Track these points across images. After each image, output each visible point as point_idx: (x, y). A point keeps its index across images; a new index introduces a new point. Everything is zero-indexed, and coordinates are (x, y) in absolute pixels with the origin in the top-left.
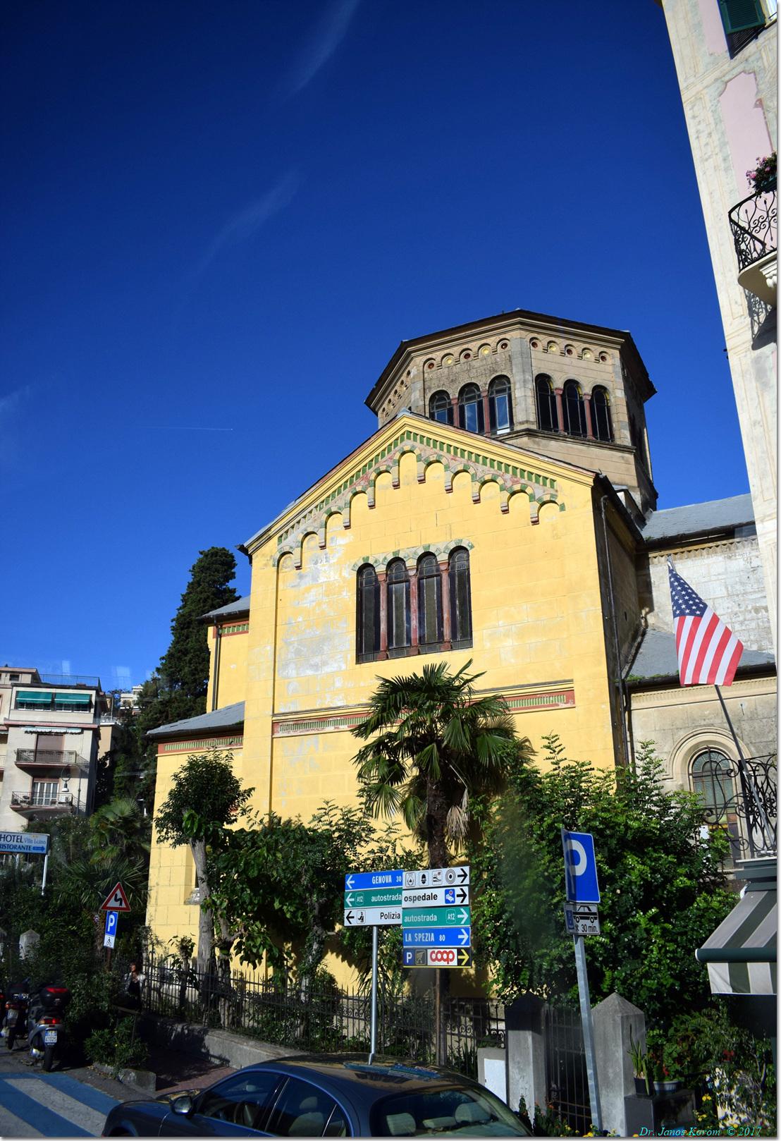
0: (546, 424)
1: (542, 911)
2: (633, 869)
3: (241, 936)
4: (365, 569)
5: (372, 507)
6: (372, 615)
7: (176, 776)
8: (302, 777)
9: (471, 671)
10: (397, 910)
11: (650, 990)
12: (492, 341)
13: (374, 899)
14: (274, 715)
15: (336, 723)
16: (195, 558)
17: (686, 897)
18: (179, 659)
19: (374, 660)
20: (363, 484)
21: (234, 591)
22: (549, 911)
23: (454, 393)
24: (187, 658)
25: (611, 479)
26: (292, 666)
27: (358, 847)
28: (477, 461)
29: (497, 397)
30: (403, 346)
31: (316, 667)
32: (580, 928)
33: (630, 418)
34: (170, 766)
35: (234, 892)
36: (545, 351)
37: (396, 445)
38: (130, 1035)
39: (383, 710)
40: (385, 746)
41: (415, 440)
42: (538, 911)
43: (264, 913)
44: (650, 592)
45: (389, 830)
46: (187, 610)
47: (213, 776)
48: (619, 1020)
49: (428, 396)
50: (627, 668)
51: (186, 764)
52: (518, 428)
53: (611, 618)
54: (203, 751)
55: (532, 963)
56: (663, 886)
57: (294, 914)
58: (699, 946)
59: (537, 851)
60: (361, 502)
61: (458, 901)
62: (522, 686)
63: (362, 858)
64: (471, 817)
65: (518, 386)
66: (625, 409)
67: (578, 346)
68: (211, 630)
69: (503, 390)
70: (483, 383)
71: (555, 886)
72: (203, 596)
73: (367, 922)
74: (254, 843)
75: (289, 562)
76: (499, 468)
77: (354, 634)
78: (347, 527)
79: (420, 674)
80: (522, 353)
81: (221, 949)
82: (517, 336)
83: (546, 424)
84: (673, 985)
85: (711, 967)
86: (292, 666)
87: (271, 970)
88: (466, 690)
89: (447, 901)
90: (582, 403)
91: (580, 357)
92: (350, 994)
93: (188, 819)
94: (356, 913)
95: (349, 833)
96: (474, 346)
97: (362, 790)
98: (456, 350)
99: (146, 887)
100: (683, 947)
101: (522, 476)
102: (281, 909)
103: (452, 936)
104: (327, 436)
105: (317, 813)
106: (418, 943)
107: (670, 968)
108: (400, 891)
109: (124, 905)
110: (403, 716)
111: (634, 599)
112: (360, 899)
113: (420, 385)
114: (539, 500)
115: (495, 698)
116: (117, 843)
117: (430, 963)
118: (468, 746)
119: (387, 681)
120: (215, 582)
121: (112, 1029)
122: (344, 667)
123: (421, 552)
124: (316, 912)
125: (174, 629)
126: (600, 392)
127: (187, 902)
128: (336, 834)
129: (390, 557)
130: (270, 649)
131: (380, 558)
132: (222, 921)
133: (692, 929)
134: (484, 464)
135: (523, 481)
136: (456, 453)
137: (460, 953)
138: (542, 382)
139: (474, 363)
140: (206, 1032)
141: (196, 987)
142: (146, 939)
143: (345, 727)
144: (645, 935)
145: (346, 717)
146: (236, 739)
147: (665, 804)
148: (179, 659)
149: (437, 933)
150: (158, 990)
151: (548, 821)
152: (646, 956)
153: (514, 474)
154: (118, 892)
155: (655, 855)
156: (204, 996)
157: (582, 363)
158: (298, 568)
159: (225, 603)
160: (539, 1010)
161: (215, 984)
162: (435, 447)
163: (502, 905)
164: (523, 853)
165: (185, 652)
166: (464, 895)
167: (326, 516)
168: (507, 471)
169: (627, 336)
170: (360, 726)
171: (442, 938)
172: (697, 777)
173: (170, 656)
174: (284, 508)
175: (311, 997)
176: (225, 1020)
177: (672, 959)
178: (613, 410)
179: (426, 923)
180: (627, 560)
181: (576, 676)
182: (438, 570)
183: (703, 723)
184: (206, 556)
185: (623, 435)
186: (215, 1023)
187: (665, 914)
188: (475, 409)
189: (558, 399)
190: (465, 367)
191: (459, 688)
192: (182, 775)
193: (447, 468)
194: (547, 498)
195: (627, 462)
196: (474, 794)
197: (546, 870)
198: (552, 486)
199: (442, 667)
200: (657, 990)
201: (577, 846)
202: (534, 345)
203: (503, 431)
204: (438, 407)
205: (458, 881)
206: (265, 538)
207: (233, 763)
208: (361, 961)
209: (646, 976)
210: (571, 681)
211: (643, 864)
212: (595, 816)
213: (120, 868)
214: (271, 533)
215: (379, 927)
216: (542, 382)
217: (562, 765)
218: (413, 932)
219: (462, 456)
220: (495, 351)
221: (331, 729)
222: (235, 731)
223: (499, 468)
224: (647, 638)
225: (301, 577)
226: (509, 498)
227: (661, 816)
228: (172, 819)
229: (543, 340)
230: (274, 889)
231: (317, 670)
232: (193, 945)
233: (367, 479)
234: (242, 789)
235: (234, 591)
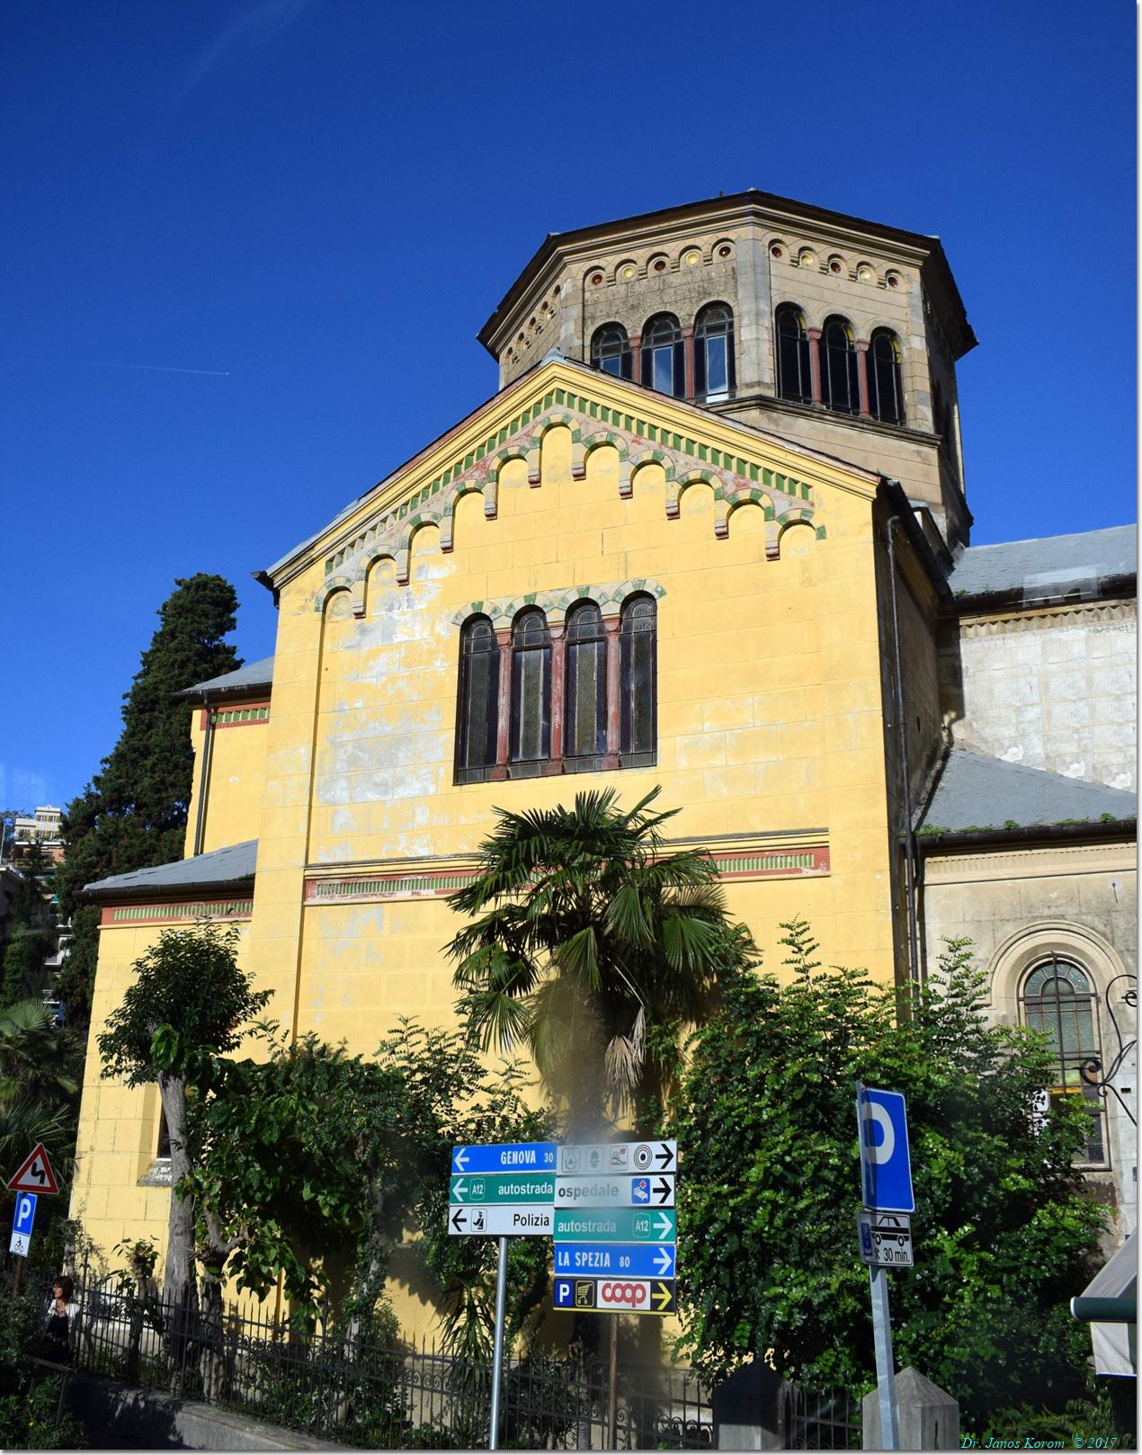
0: (791, 388)
1: (778, 1222)
2: (935, 1156)
3: (242, 1245)
4: (475, 623)
5: (491, 516)
6: (483, 703)
7: (139, 964)
8: (361, 977)
9: (658, 806)
10: (547, 1211)
11: (957, 1364)
12: (705, 241)
13: (502, 1190)
14: (307, 867)
15: (415, 885)
16: (167, 592)
17: (1021, 1208)
18: (134, 762)
19: (486, 779)
20: (478, 476)
21: (232, 651)
22: (788, 1223)
23: (634, 329)
24: (149, 762)
25: (907, 490)
26: (343, 783)
27: (455, 1100)
28: (676, 446)
29: (709, 339)
30: (550, 244)
31: (384, 787)
32: (882, 1255)
33: (933, 386)
34: (125, 950)
35: (232, 1167)
36: (795, 263)
37: (537, 412)
38: (53, 1408)
39: (506, 866)
40: (503, 926)
41: (570, 405)
42: (771, 1223)
43: (283, 1206)
44: (960, 685)
45: (510, 1072)
46: (150, 679)
47: (204, 967)
48: (917, 1413)
49: (591, 330)
50: (918, 812)
51: (157, 944)
52: (743, 393)
53: (896, 727)
54: (187, 923)
55: (756, 1311)
56: (980, 1188)
57: (335, 1210)
58: (1078, 1293)
59: (771, 1121)
60: (473, 507)
61: (656, 1199)
62: (740, 837)
63: (460, 1119)
64: (648, 1055)
65: (745, 321)
66: (926, 370)
67: (850, 258)
68: (198, 716)
69: (719, 328)
70: (686, 313)
71: (802, 1180)
72: (180, 656)
73: (489, 1230)
74: (271, 1088)
75: (343, 606)
76: (715, 461)
77: (453, 733)
78: (447, 550)
79: (570, 808)
80: (754, 266)
81: (208, 1265)
82: (747, 236)
83: (791, 388)
84: (995, 1357)
85: (1096, 1328)
86: (343, 783)
87: (285, 1305)
88: (648, 838)
89: (636, 1199)
90: (853, 357)
91: (853, 277)
92: (420, 1352)
93: (161, 1039)
94: (470, 1213)
95: (439, 1074)
96: (672, 249)
97: (465, 1003)
98: (641, 255)
99: (72, 1152)
100: (1011, 1293)
101: (754, 477)
102: (313, 1201)
103: (643, 1259)
104: (412, 394)
105: (390, 1038)
106: (580, 1270)
107: (991, 1329)
108: (550, 1179)
109: (47, 1184)
110: (536, 876)
111: (932, 696)
112: (478, 1189)
113: (576, 311)
114: (782, 518)
115: (698, 853)
116: (15, 1075)
117: (601, 1303)
118: (649, 934)
119: (512, 817)
120: (200, 633)
121: (22, 1394)
122: (432, 790)
123: (573, 598)
124: (378, 1208)
125: (126, 711)
126: (884, 338)
127: (143, 1182)
128: (419, 1077)
129: (519, 605)
130: (304, 752)
131: (502, 607)
132: (209, 1217)
133: (1029, 1263)
134: (689, 451)
135: (754, 485)
136: (640, 431)
137: (655, 1288)
138: (788, 315)
139: (671, 278)
140: (178, 1407)
141: (158, 1328)
142: (71, 1241)
143: (430, 893)
144: (951, 1271)
145: (432, 876)
146: (238, 905)
147: (986, 1049)
148: (134, 762)
149: (616, 1253)
150: (87, 1331)
151: (792, 1068)
152: (949, 1307)
153: (741, 472)
154: (39, 1160)
155: (971, 1134)
156: (174, 1344)
157: (855, 288)
158: (359, 615)
159: (216, 674)
160: (775, 1391)
161: (194, 1328)
162: (604, 418)
163: (709, 1208)
164: (747, 1121)
165: (145, 753)
166: (667, 1190)
167: (410, 528)
168: (728, 466)
169: (934, 245)
170: (462, 893)
171: (625, 1262)
172: (1032, 1004)
173: (119, 758)
174: (340, 510)
175: (362, 1351)
176: (211, 1387)
177: (995, 1313)
178: (905, 371)
179: (596, 1235)
180: (923, 628)
181: (835, 823)
182: (601, 631)
183: (1046, 912)
184: (188, 588)
185: (921, 416)
186: (193, 1392)
187: (982, 1238)
188: (669, 354)
189: (813, 349)
190: (656, 285)
191: (635, 835)
192: (151, 964)
193: (624, 456)
194: (795, 515)
195: (926, 461)
196: (655, 1017)
197: (788, 1152)
198: (805, 496)
199: (608, 797)
200: (969, 1366)
201: (880, 1113)
202: (776, 252)
203: (717, 397)
204: (606, 351)
205: (656, 1165)
206: (303, 562)
207: (238, 947)
208: (448, 1299)
209: (950, 1339)
210: (825, 830)
211: (951, 1149)
212: (875, 1064)
213: (27, 1119)
214: (314, 553)
215: (510, 1238)
216: (788, 315)
217: (813, 973)
218: (572, 1249)
219: (652, 437)
220: (708, 261)
221: (406, 894)
222: (241, 890)
223: (715, 461)
224: (951, 762)
225: (364, 631)
226: (730, 514)
227: (980, 1067)
228: (130, 1039)
229: (792, 244)
230: (302, 1165)
231: (385, 792)
232: (154, 1256)
233: (484, 467)
234: (252, 991)
235: (232, 651)
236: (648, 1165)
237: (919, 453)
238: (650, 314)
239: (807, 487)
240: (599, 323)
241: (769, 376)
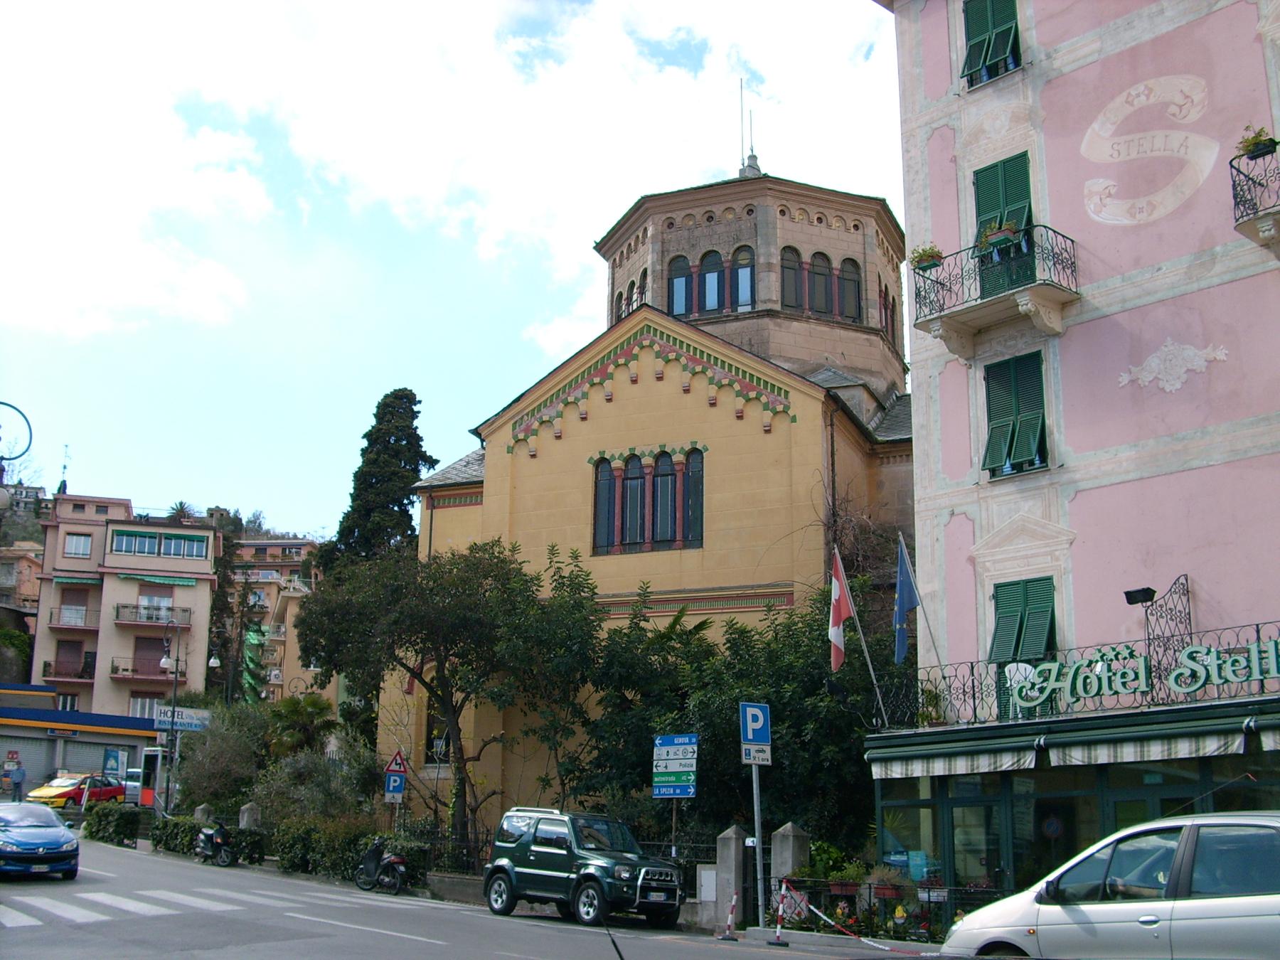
4: (601, 463)
13: (680, 284)
41: (655, 335)
49: (667, 259)
131: (616, 452)
182: (673, 469)
238: (704, 251)
240: (672, 255)
241: (775, 295)
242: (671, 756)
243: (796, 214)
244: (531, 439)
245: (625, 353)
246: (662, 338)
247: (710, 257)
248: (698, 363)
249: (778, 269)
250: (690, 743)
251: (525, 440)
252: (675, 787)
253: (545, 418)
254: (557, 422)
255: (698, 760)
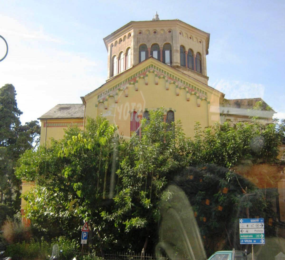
0: (184, 65)
41: (155, 68)
49: (139, 45)
70: (161, 45)
83: (184, 65)
138: (182, 47)
216: (182, 47)
236: (258, 227)
237: (205, 80)
238: (153, 43)
239: (206, 93)
240: (167, 42)
241: (179, 61)
242: (250, 227)
243: (184, 34)
244: (106, 103)
245: (144, 74)
246: (157, 70)
247: (155, 46)
248: (174, 80)
249: (179, 52)
250: (260, 222)
251: (103, 102)
252: (253, 240)
253: (111, 95)
254: (116, 96)
255: (265, 228)
